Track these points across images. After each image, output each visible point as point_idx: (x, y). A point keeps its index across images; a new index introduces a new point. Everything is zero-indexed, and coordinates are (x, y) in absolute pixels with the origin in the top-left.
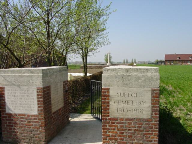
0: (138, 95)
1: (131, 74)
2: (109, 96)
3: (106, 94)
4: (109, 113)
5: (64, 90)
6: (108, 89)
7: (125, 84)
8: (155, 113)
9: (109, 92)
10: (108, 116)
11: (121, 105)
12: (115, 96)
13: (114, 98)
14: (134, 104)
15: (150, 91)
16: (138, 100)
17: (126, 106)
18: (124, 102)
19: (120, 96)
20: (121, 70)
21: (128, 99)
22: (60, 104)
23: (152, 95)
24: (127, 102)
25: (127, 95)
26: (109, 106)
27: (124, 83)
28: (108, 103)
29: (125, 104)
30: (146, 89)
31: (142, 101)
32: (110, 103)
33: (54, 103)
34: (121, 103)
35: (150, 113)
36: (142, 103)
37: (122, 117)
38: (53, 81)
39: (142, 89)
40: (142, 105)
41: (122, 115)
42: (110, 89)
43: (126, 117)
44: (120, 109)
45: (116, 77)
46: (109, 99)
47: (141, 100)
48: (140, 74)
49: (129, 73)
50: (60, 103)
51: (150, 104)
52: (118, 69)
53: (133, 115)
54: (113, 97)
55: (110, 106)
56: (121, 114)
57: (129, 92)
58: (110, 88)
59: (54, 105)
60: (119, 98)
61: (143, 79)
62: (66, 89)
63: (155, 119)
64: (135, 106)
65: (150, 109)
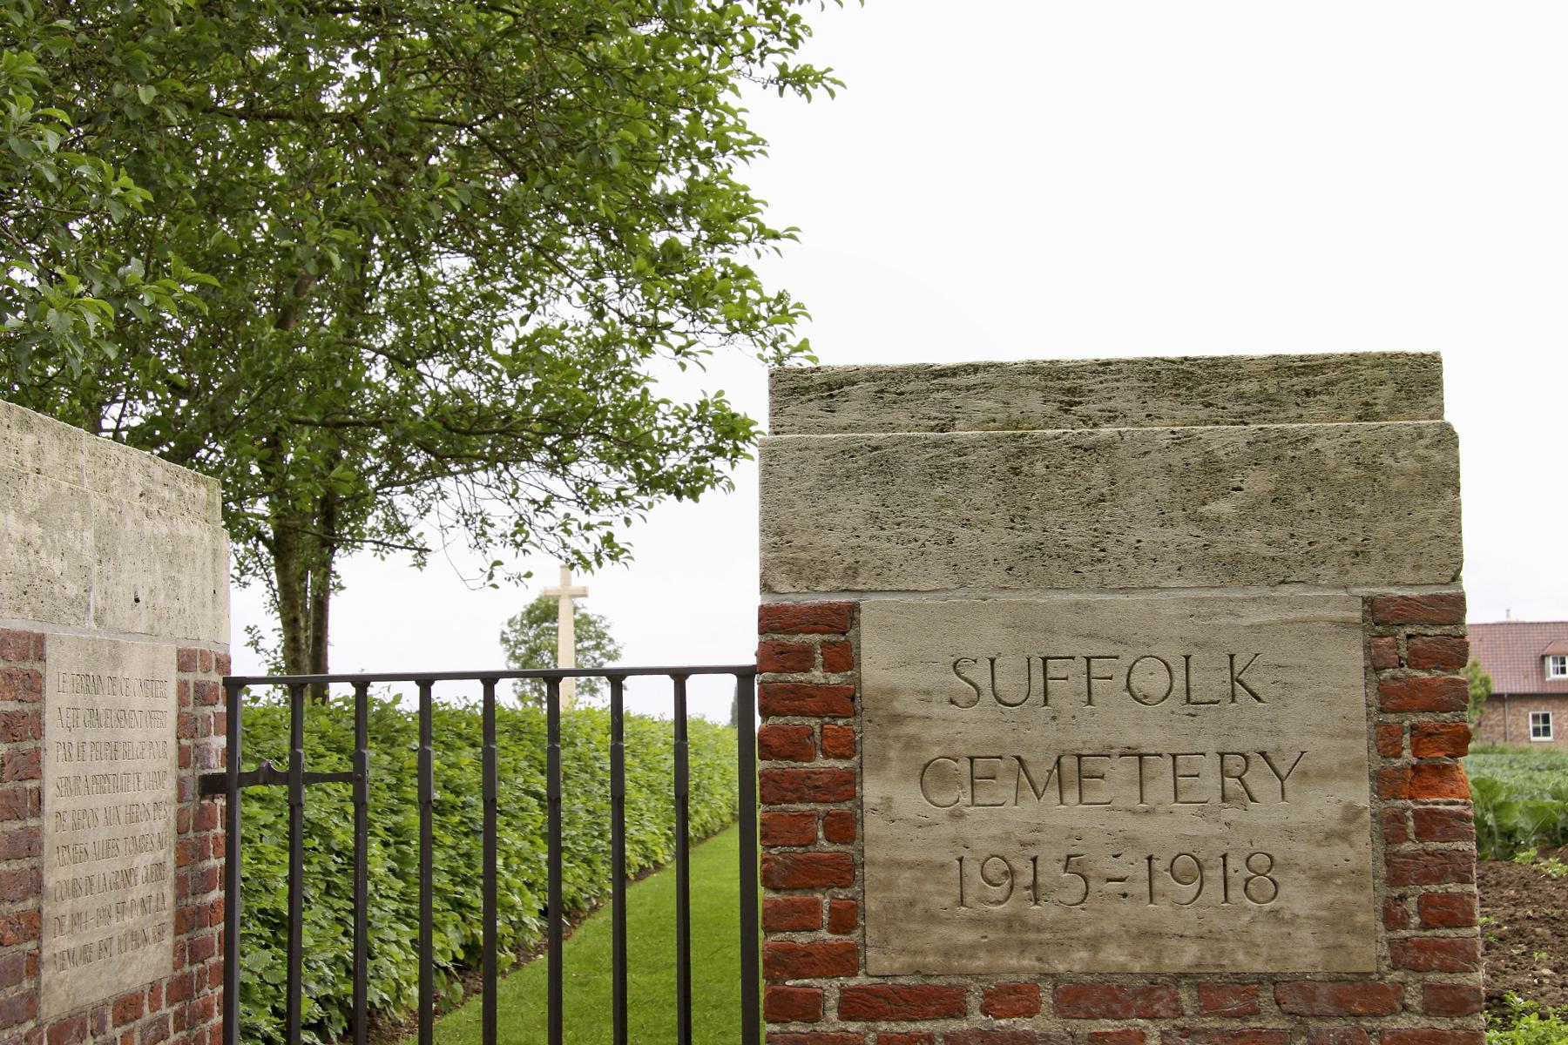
0: (1210, 680)
1: (1106, 431)
2: (845, 702)
3: (817, 675)
4: (844, 920)
5: (184, 759)
6: (836, 610)
7: (1039, 546)
8: (1426, 902)
9: (844, 658)
10: (846, 961)
11: (1001, 816)
12: (927, 695)
13: (910, 729)
14: (1160, 790)
15: (1346, 624)
16: (1212, 746)
17: (1064, 814)
18: (1039, 773)
19: (988, 696)
20: (988, 387)
21: (1087, 734)
22: (137, 938)
23: (1378, 670)
24: (1075, 771)
25: (1066, 691)
26: (845, 828)
27: (1029, 537)
28: (846, 786)
29: (1053, 794)
30: (1301, 603)
31: (1263, 754)
32: (872, 790)
33: (74, 889)
34: (1004, 790)
35: (1366, 908)
36: (1261, 782)
37: (1018, 965)
38: (72, 590)
39: (1254, 609)
40: (1270, 811)
41: (1024, 947)
42: (865, 617)
43: (1076, 961)
44: (995, 868)
45: (940, 474)
46: (846, 747)
47: (1247, 742)
48: (1225, 438)
49: (1085, 420)
50: (131, 920)
51: (1362, 795)
52: (954, 371)
53: (1148, 935)
54: (897, 719)
55: (872, 826)
56: (1009, 923)
57: (1096, 648)
58: (867, 602)
59: (77, 917)
60: (974, 727)
61: (1258, 482)
62: (202, 755)
63: (1431, 977)
64: (1176, 826)
65: (1362, 852)
